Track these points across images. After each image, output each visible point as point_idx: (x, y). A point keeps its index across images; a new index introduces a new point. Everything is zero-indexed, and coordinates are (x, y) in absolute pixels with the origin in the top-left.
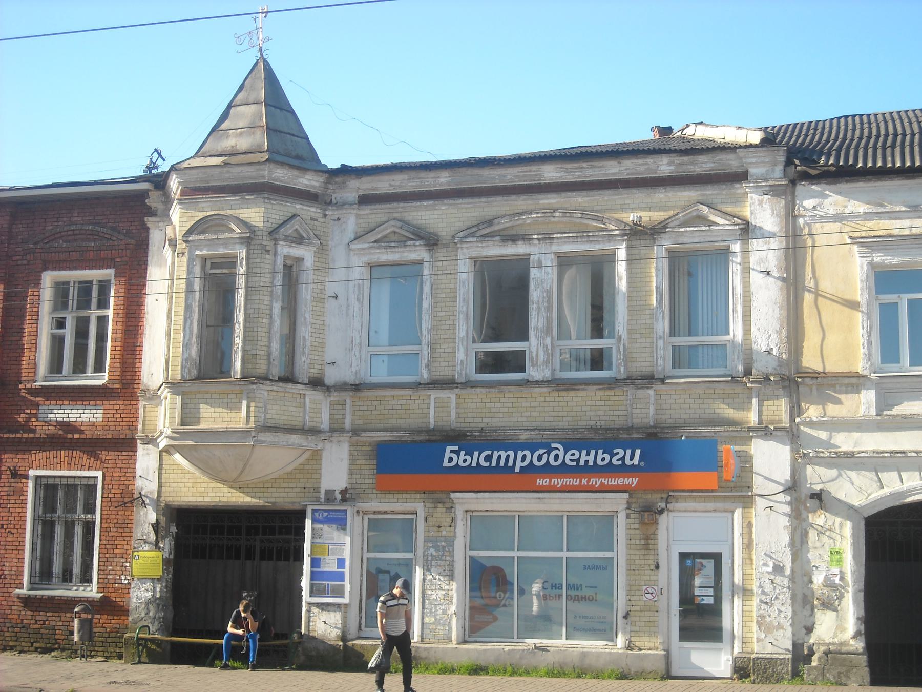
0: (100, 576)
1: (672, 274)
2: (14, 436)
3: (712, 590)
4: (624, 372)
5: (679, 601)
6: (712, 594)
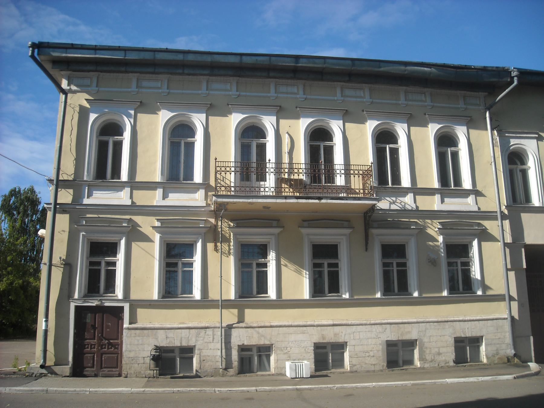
0: (259, 164)
3: (62, 269)
5: (148, 236)
6: (290, 195)
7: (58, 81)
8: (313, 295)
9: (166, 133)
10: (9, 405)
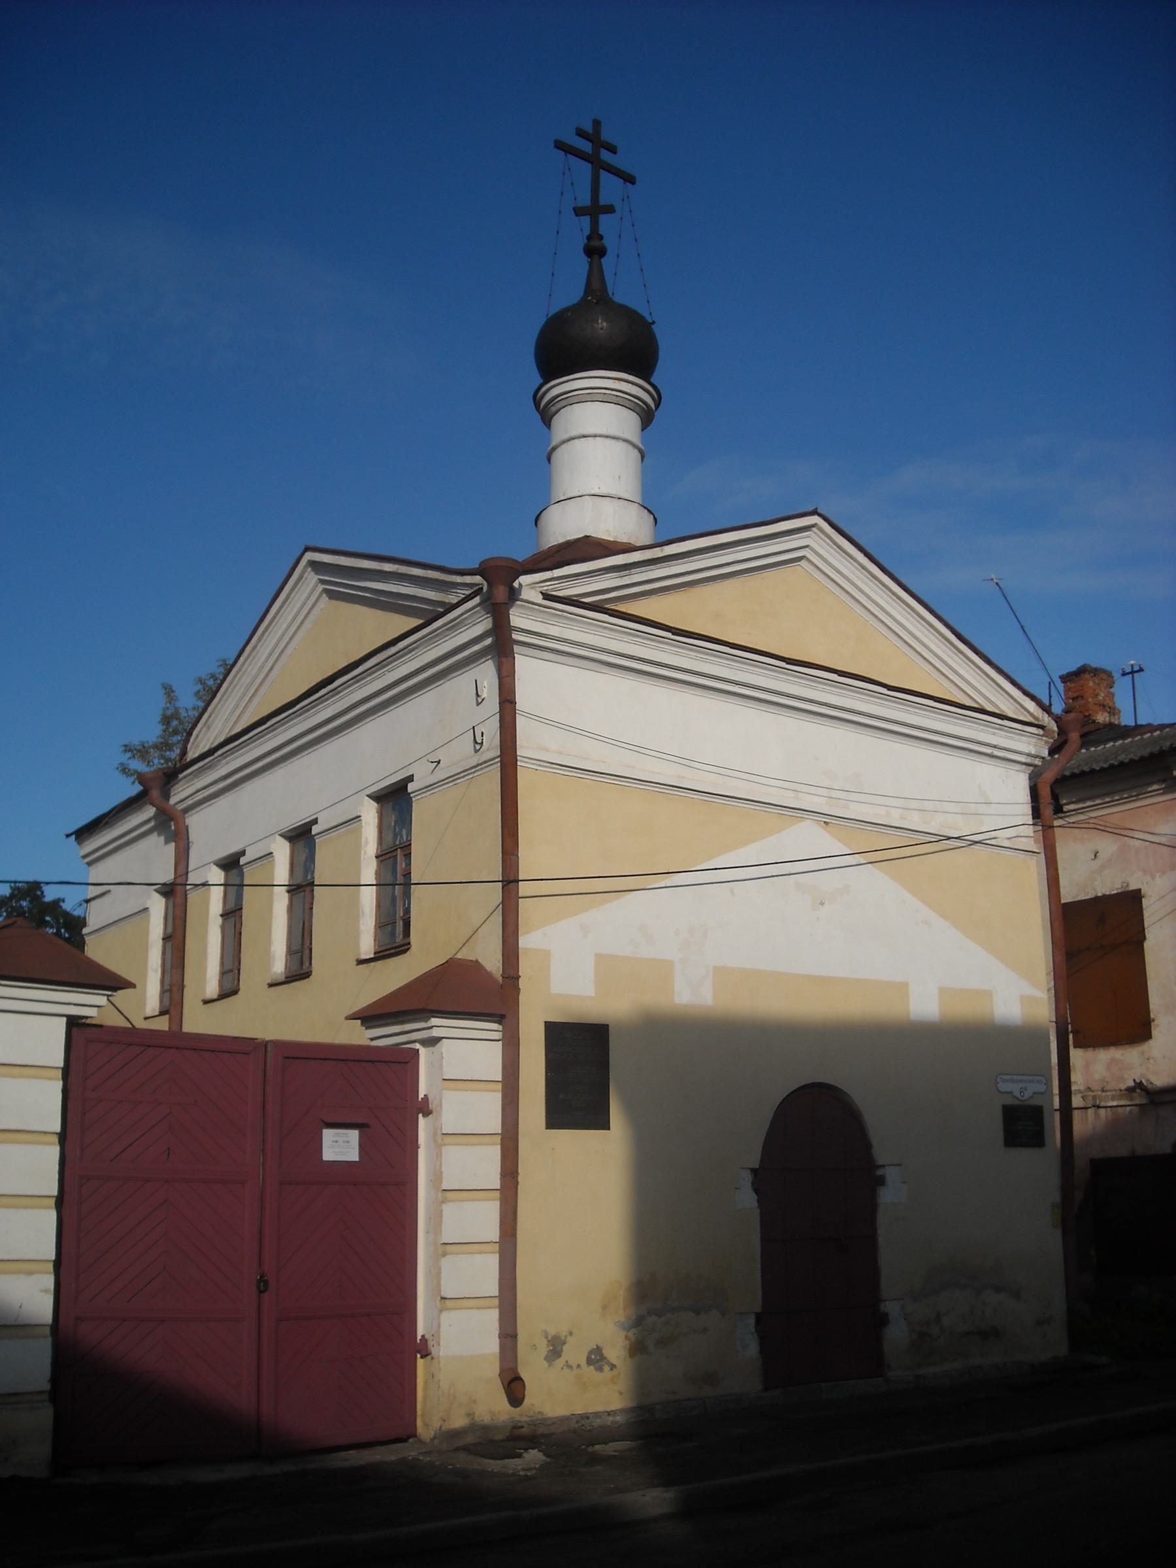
1: (298, 977)
2: (1071, 1036)
4: (1127, 743)
7: (149, 949)
8: (547, 1024)
9: (900, 614)
10: (569, 315)
